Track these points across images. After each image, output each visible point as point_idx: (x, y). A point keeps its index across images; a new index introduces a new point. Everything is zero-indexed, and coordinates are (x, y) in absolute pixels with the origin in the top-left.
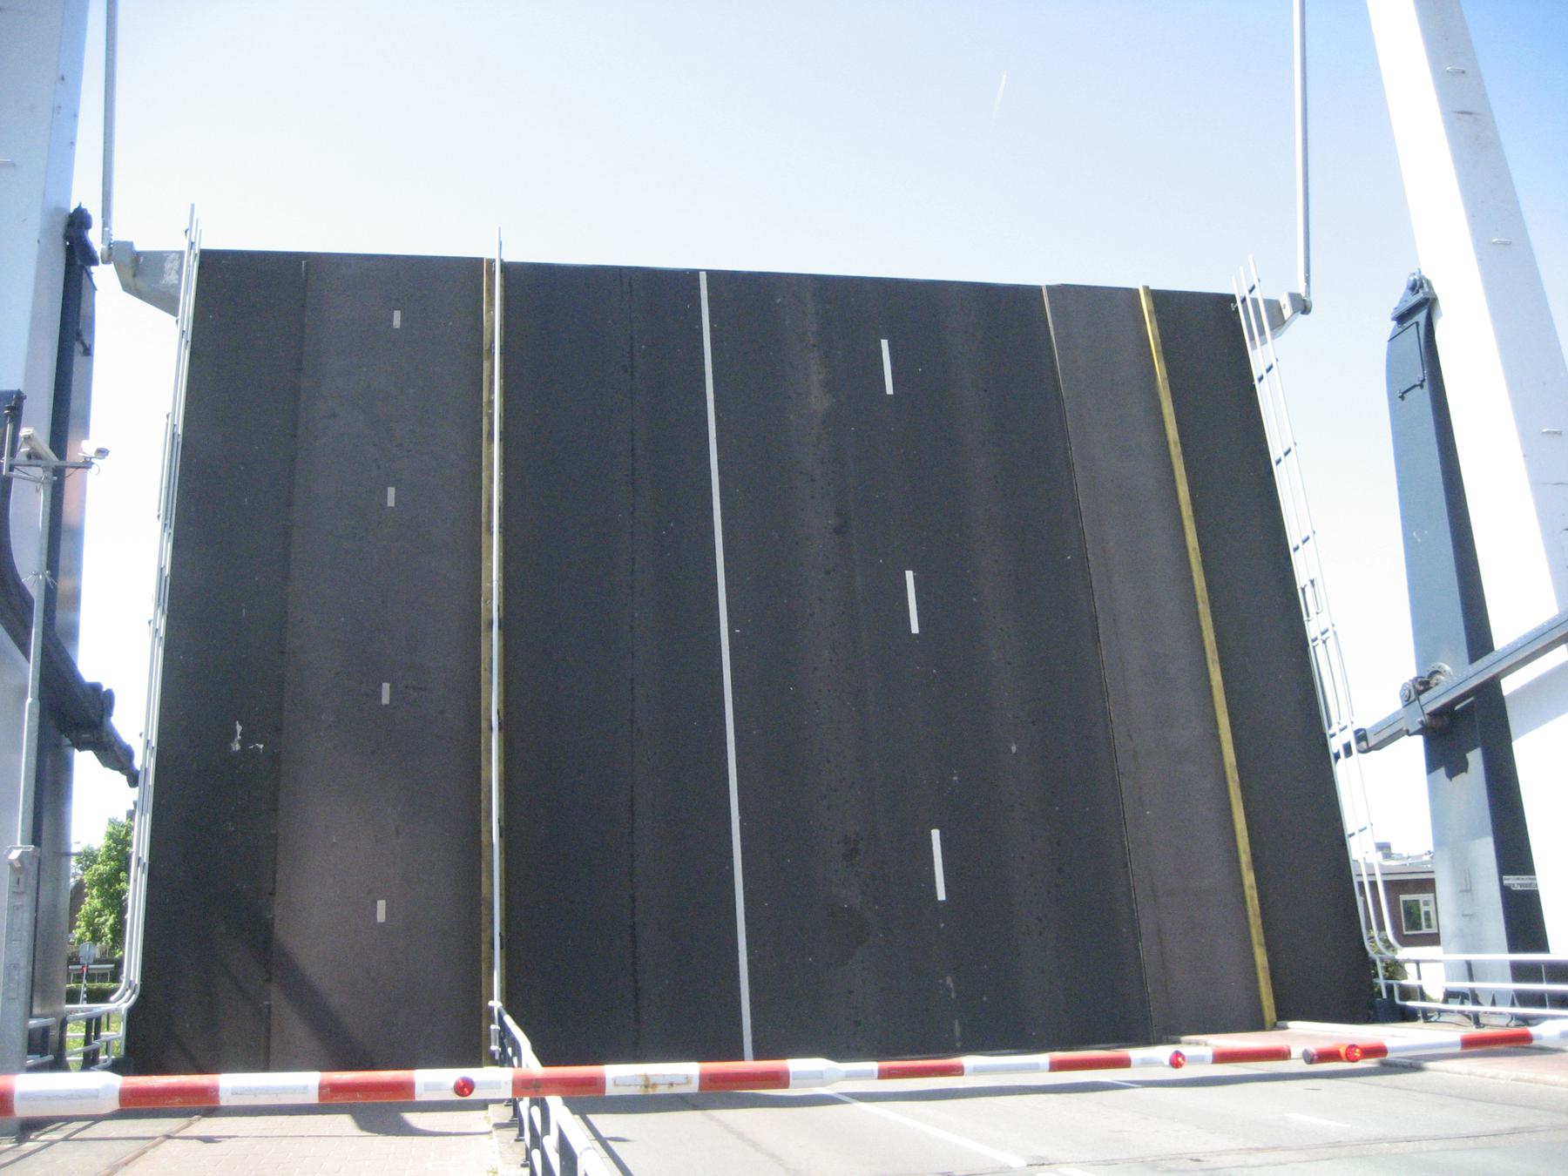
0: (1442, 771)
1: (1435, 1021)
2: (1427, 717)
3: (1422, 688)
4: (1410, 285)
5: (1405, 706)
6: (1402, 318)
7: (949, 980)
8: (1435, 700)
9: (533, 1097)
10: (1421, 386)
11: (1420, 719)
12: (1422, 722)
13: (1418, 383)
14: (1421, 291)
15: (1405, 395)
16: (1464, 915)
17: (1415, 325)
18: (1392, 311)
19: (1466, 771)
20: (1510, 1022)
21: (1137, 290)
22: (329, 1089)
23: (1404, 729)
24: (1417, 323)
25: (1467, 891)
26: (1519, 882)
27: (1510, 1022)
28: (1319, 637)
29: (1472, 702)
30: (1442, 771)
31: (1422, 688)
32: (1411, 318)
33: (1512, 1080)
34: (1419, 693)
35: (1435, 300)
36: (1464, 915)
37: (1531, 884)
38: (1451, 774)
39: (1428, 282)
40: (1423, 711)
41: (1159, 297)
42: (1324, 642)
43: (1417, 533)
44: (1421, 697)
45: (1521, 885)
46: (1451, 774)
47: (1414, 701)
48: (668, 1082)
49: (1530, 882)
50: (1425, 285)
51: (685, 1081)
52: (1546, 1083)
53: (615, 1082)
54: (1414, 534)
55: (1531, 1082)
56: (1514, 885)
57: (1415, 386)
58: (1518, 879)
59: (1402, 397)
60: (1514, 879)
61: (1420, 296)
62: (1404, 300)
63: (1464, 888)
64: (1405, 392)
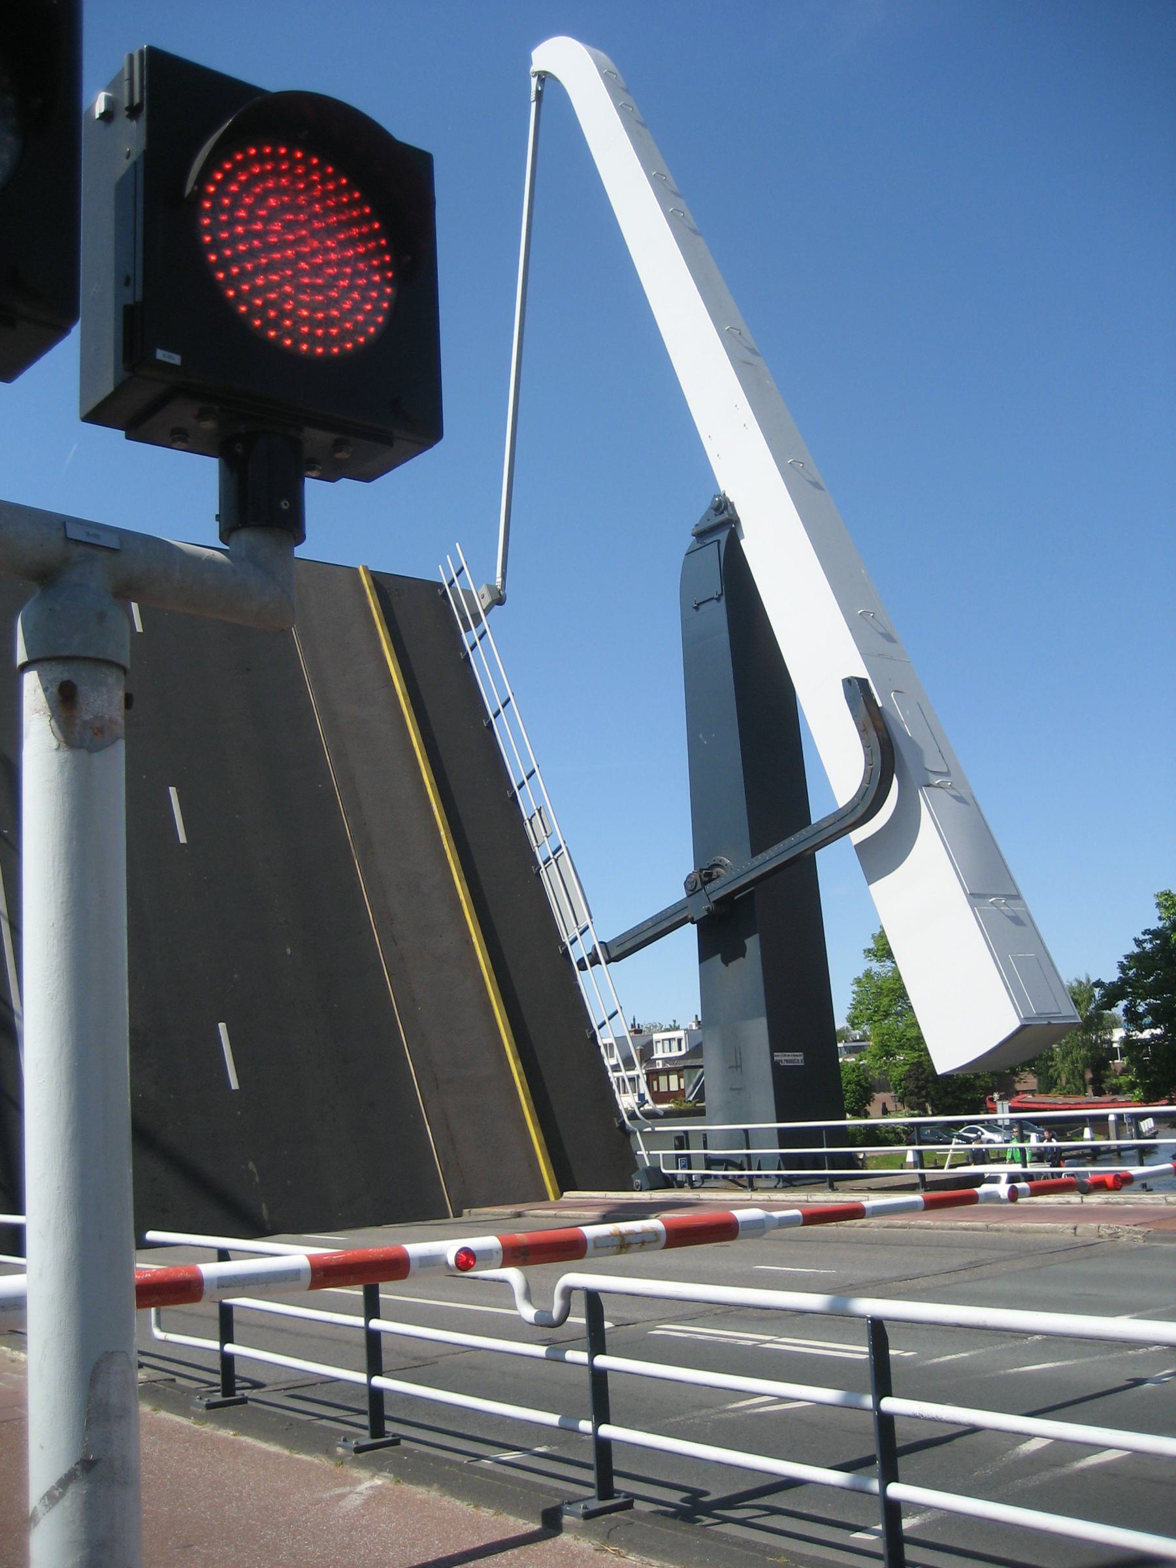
0: (718, 958)
1: (700, 1187)
2: (712, 904)
3: (707, 879)
4: (716, 505)
5: (689, 896)
6: (701, 535)
7: (251, 1165)
8: (718, 890)
9: (367, 1284)
10: (718, 599)
11: (702, 908)
12: (708, 910)
13: (716, 596)
14: (725, 512)
15: (700, 607)
16: (732, 1089)
17: (716, 543)
18: (693, 527)
19: (744, 957)
20: (778, 1184)
21: (357, 570)
22: (322, 1273)
23: (690, 916)
24: (719, 541)
25: (737, 1067)
26: (785, 1058)
27: (778, 1184)
28: (552, 856)
29: (752, 890)
30: (718, 958)
31: (707, 879)
32: (713, 536)
33: (884, 1227)
34: (704, 883)
35: (737, 521)
36: (732, 1089)
37: (794, 1060)
38: (726, 961)
39: (732, 505)
40: (709, 900)
41: (378, 579)
42: (556, 860)
43: (703, 735)
44: (707, 887)
45: (787, 1061)
46: (726, 961)
47: (701, 889)
48: (640, 1241)
49: (794, 1058)
50: (729, 508)
51: (654, 1238)
52: (921, 1227)
53: (595, 1244)
54: (701, 736)
55: (905, 1228)
56: (781, 1061)
57: (712, 599)
58: (785, 1056)
59: (697, 608)
60: (781, 1056)
61: (725, 516)
62: (706, 518)
63: (734, 1064)
64: (699, 604)
